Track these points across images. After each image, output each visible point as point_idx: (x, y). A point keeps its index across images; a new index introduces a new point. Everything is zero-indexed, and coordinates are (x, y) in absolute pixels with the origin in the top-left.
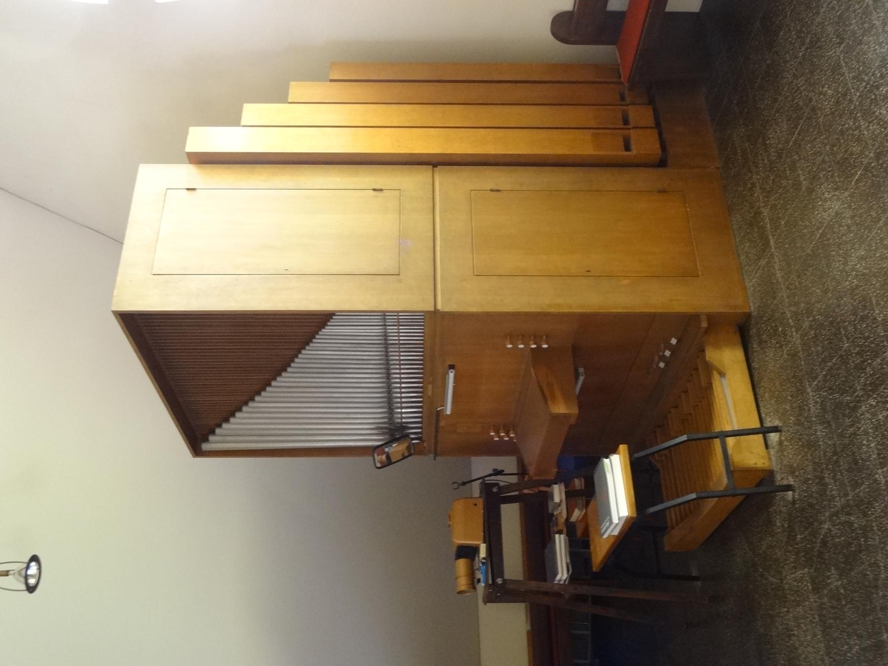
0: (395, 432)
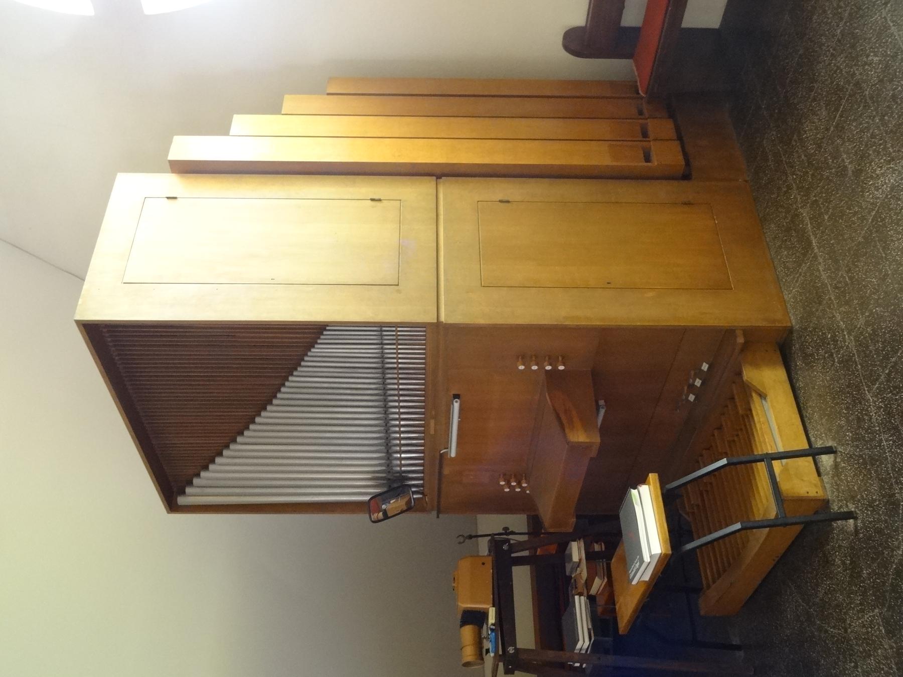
0: (394, 484)
